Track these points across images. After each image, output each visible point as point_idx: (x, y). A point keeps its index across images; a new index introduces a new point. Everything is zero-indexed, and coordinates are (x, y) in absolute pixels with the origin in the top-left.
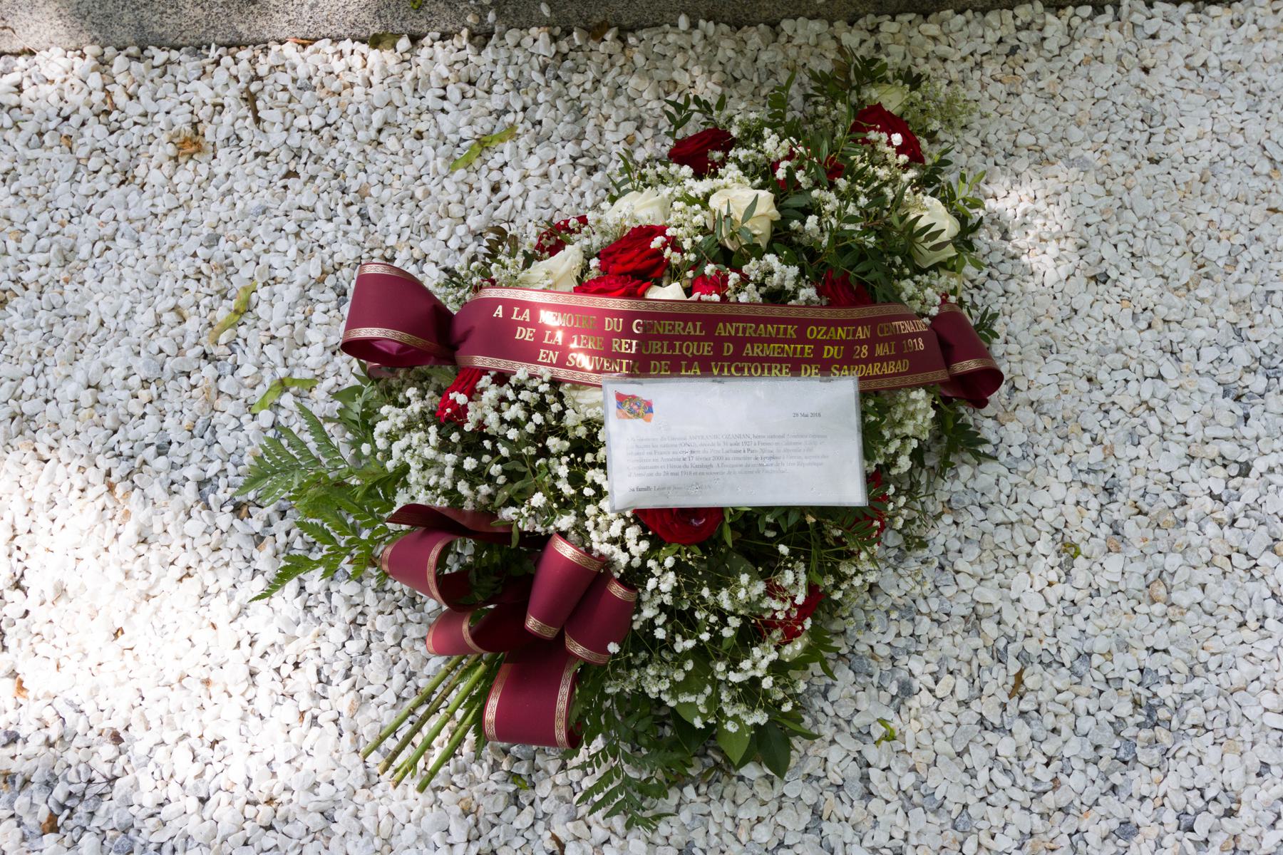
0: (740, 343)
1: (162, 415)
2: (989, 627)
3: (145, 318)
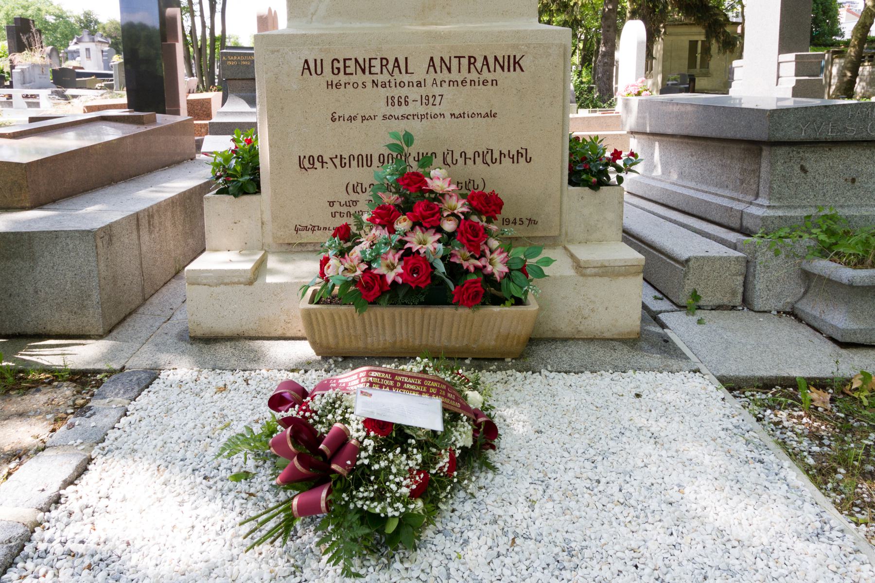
0: (403, 383)
1: (186, 451)
2: (500, 522)
3: (191, 425)
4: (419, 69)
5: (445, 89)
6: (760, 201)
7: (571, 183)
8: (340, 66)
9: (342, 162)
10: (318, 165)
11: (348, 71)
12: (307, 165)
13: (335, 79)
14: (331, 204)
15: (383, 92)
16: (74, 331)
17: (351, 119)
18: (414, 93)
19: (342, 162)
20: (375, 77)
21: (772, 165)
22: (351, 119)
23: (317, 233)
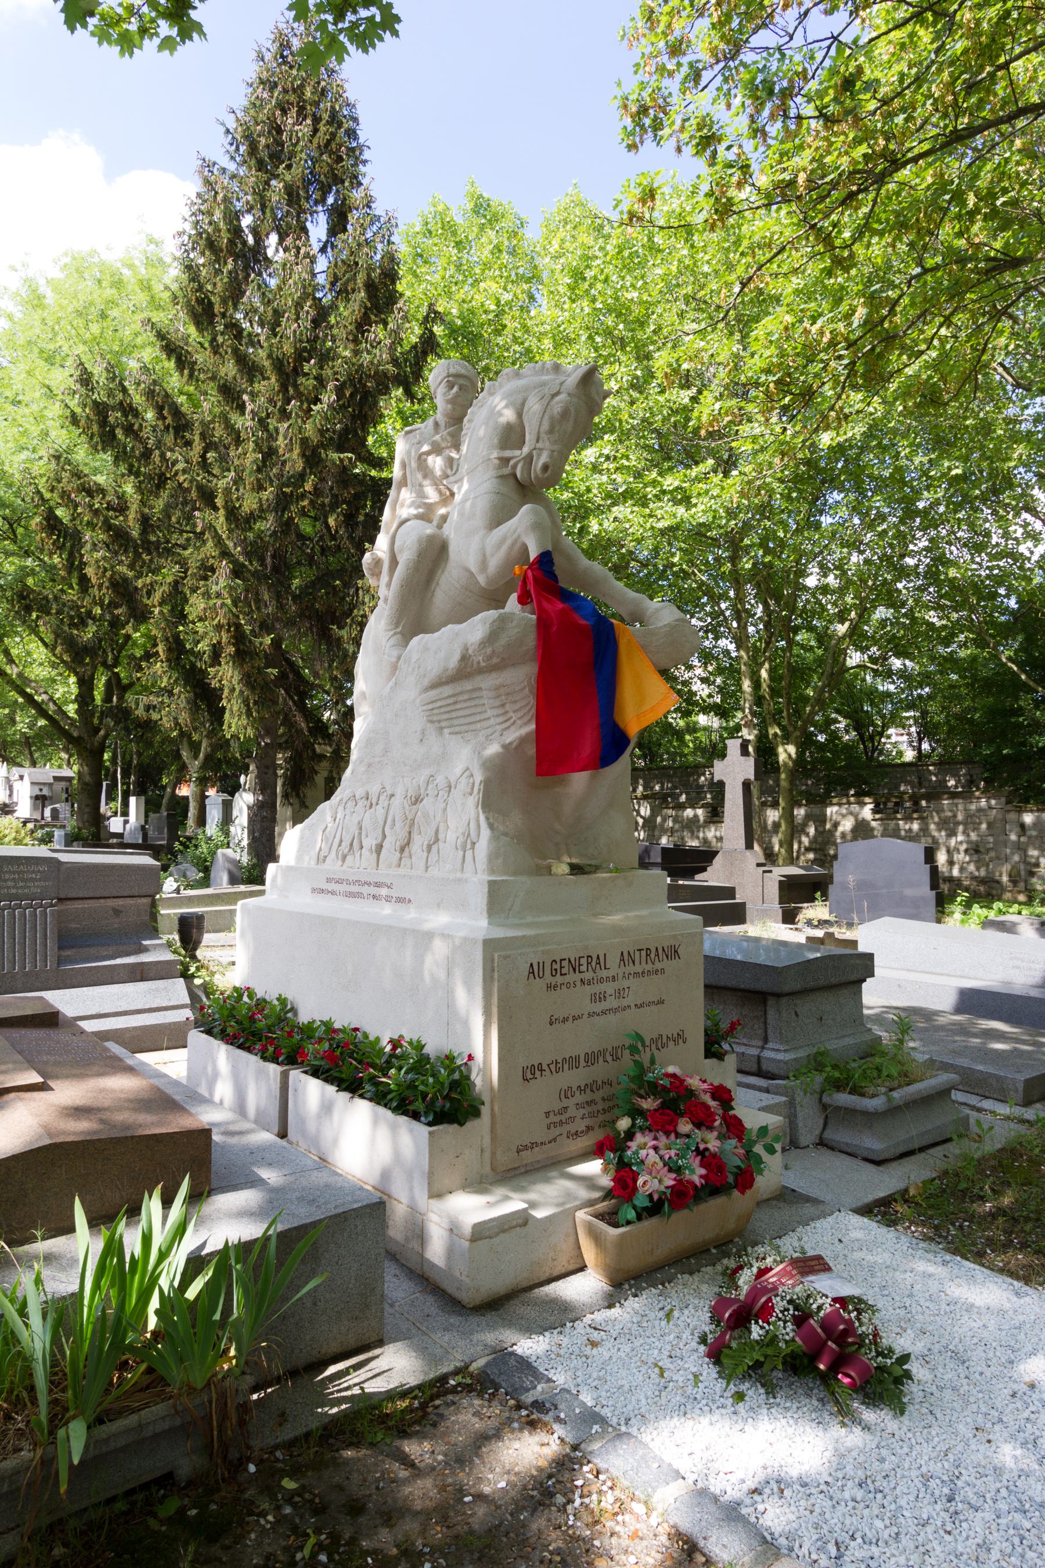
4: (613, 961)
5: (632, 982)
6: (770, 1045)
7: (706, 1057)
8: (558, 967)
9: (557, 1066)
10: (538, 1073)
11: (564, 971)
12: (529, 1076)
13: (553, 980)
14: (547, 1114)
15: (589, 990)
16: (352, 1343)
17: (565, 1020)
18: (609, 988)
19: (557, 1066)
20: (582, 976)
21: (779, 1011)
22: (565, 1020)
23: (536, 1150)
